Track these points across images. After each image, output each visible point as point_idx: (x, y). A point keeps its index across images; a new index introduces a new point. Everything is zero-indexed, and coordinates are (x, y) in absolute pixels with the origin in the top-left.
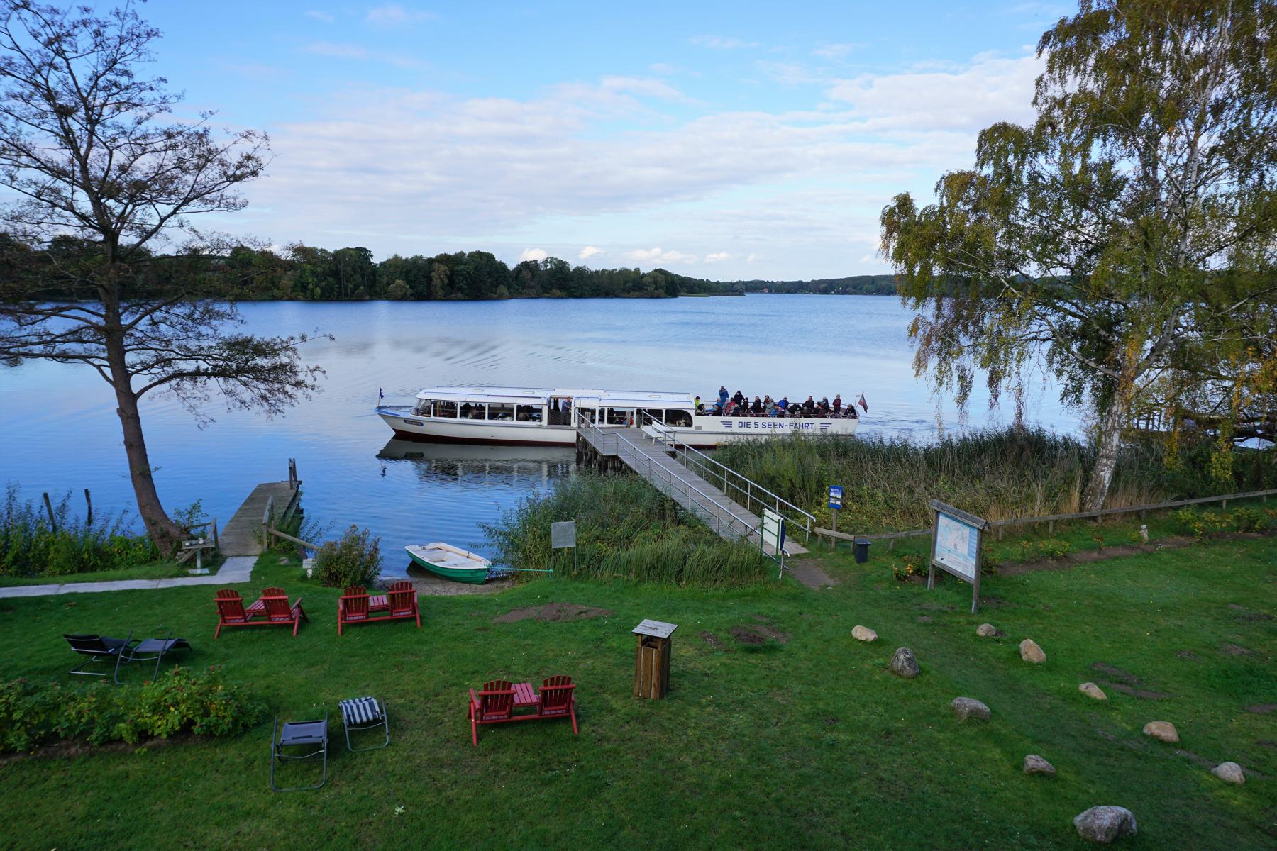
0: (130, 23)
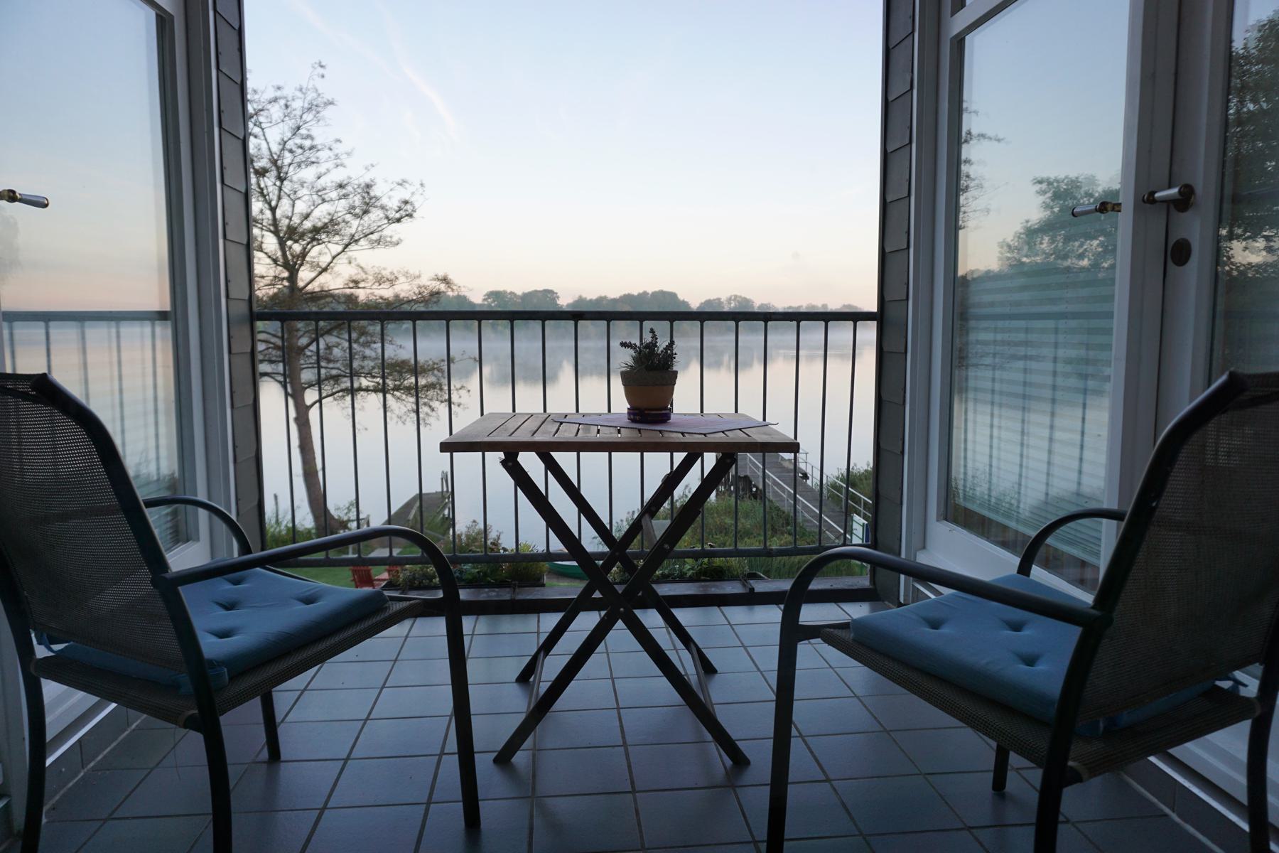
0: (311, 95)
